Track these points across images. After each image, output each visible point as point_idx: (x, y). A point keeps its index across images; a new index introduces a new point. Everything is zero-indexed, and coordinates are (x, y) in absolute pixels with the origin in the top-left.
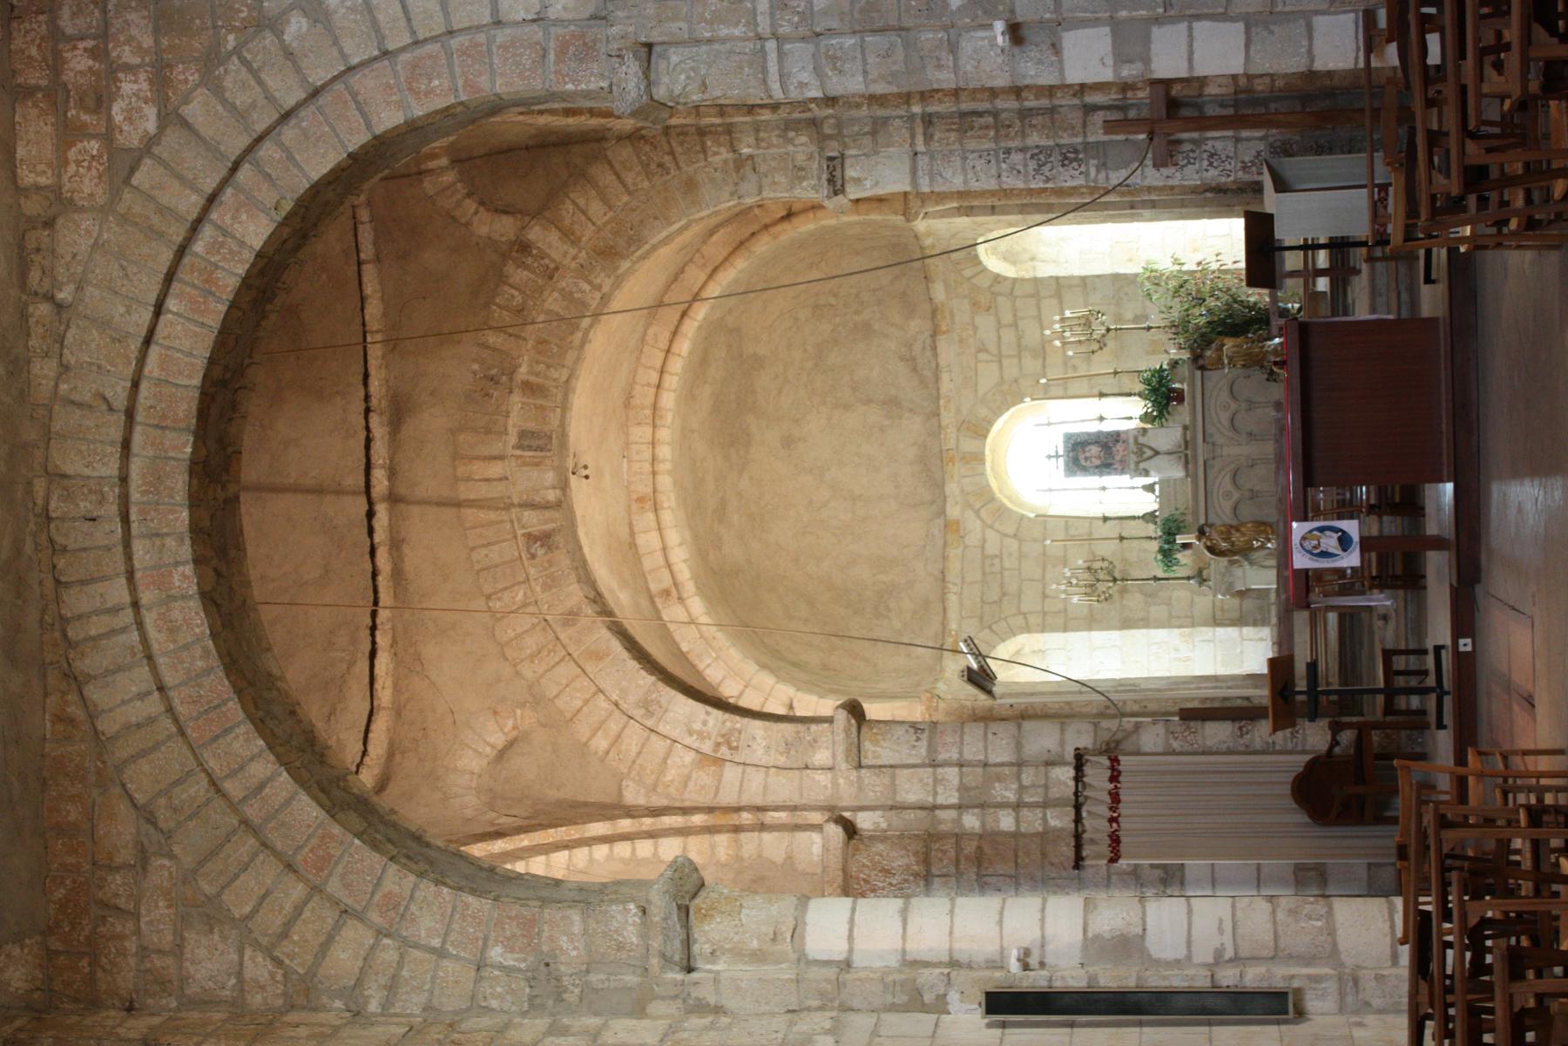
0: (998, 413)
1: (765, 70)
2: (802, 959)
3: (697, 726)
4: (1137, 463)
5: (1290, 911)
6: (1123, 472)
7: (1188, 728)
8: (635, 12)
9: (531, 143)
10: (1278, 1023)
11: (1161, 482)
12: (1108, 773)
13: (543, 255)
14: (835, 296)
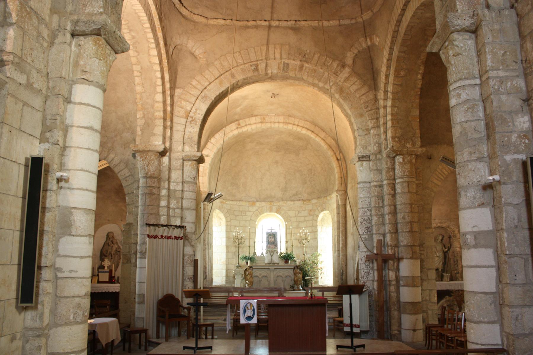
0: (282, 216)
1: (466, 79)
2: (74, 82)
3: (198, 111)
5: (80, 304)
6: (267, 247)
7: (192, 262)
8: (495, 21)
9: (374, 69)
10: (17, 298)
11: (264, 257)
12: (177, 236)
13: (341, 72)
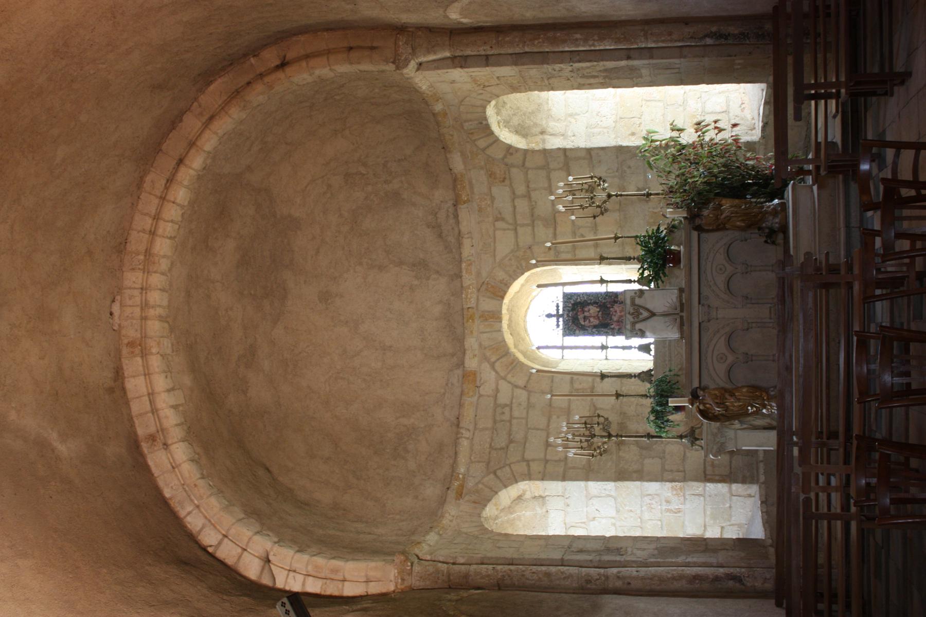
0: (514, 277)
4: (633, 324)
6: (619, 332)
14: (365, 165)
